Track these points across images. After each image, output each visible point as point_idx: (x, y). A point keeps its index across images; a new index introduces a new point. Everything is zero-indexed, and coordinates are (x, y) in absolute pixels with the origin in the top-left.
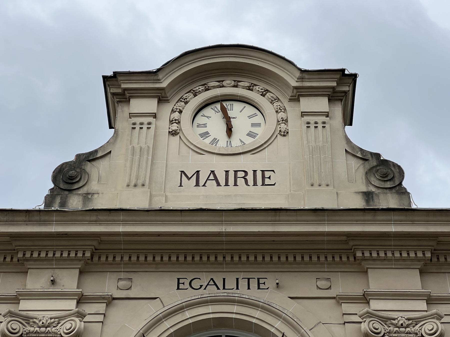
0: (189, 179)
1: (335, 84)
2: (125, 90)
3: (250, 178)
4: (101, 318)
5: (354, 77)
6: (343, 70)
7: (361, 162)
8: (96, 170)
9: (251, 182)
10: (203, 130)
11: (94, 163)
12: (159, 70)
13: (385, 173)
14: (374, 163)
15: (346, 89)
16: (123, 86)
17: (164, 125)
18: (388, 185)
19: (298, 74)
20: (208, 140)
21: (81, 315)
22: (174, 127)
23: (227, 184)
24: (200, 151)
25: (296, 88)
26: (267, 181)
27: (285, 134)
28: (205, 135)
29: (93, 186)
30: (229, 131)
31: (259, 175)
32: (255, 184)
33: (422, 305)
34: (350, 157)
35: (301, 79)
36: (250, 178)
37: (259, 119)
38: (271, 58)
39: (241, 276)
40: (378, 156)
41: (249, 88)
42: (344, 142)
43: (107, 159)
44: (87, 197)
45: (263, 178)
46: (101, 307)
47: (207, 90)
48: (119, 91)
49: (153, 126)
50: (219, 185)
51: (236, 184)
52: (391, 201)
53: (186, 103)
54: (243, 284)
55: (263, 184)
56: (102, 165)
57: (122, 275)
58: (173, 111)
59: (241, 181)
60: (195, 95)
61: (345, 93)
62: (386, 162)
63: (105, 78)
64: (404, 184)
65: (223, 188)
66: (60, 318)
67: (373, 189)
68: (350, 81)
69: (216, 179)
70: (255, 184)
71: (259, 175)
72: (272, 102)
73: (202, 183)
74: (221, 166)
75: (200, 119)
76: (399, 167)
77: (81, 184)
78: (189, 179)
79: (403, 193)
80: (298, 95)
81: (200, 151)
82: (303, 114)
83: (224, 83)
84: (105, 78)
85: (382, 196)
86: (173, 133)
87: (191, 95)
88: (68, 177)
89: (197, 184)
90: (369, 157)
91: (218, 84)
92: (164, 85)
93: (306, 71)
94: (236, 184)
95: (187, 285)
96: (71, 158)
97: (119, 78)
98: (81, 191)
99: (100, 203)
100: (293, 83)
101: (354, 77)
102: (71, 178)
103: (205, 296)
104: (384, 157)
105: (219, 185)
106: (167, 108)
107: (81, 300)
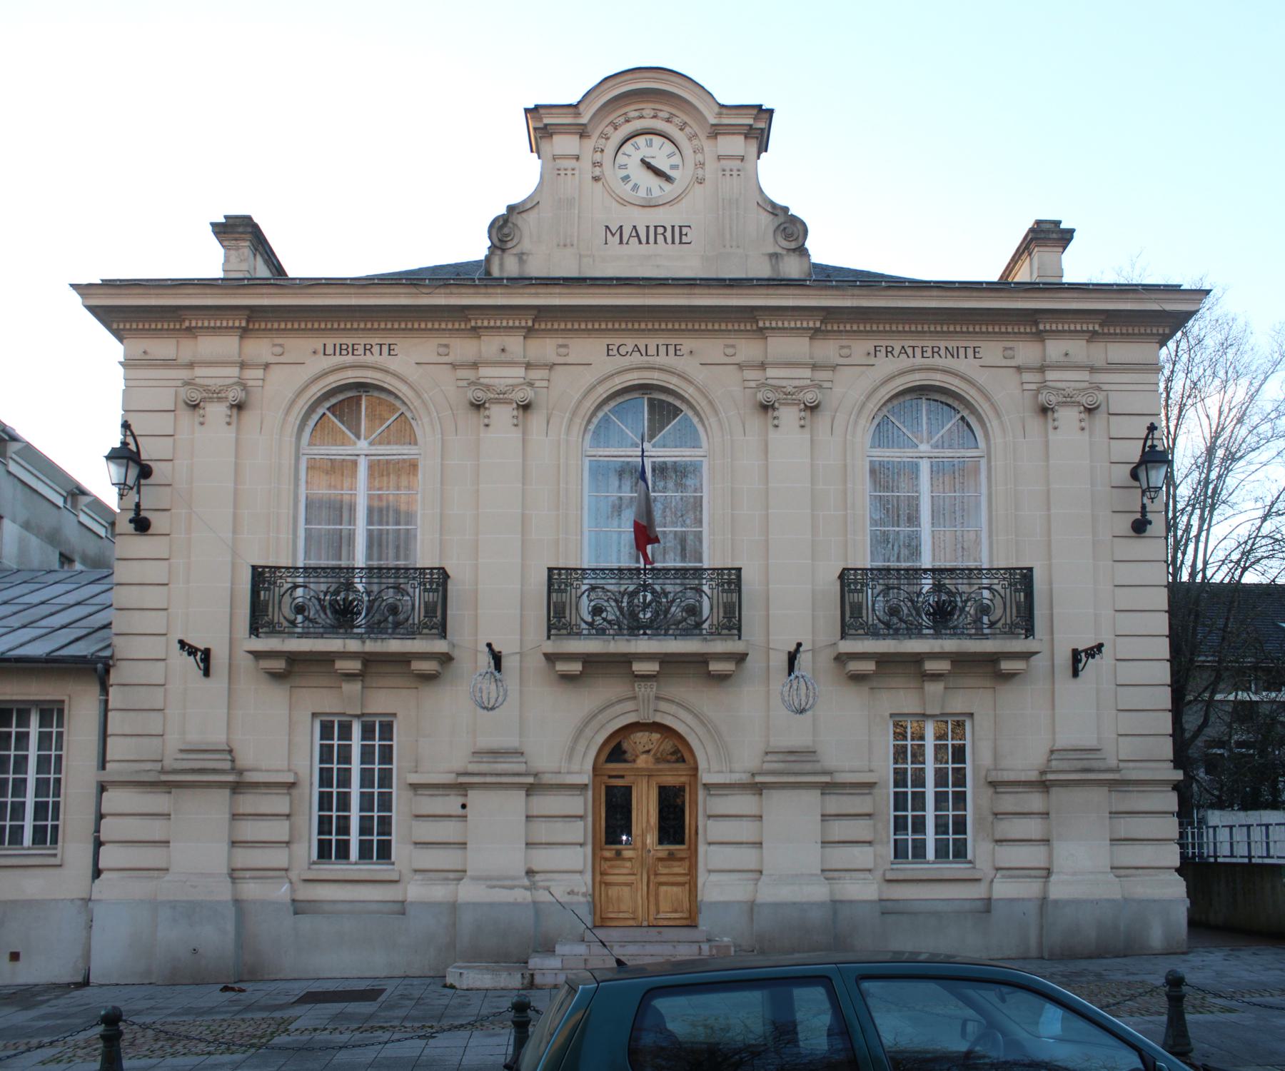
0: (613, 235)
1: (751, 121)
2: (546, 125)
3: (669, 234)
4: (545, 384)
5: (771, 112)
6: (761, 106)
7: (772, 217)
8: (528, 223)
9: (669, 240)
10: (623, 173)
11: (524, 215)
12: (579, 102)
13: (791, 229)
14: (781, 219)
15: (762, 125)
16: (546, 121)
17: (586, 164)
18: (793, 245)
19: (717, 109)
20: (630, 185)
21: (531, 385)
22: (597, 172)
23: (648, 242)
24: (624, 203)
25: (713, 125)
26: (684, 239)
27: (701, 182)
28: (626, 179)
29: (526, 245)
30: (649, 166)
31: (677, 230)
32: (673, 242)
33: (807, 373)
34: (761, 210)
35: (720, 115)
36: (669, 234)
37: (676, 160)
38: (691, 86)
39: (661, 342)
40: (786, 209)
41: (668, 120)
42: (758, 192)
43: (535, 211)
44: (521, 257)
45: (679, 235)
46: (542, 373)
47: (628, 121)
48: (541, 125)
49: (576, 172)
50: (640, 242)
51: (656, 242)
52: (792, 268)
53: (607, 139)
54: (662, 350)
55: (681, 243)
56: (531, 217)
57: (561, 341)
58: (595, 151)
59: (660, 238)
60: (616, 129)
61: (762, 130)
62: (795, 220)
63: (527, 110)
64: (807, 245)
65: (644, 246)
66: (513, 386)
67: (779, 250)
68: (767, 116)
69: (638, 236)
70: (673, 242)
71: (677, 230)
72: (690, 139)
73: (625, 240)
74: (644, 219)
75: (621, 159)
76: (803, 224)
77: (514, 242)
78: (613, 235)
79: (802, 251)
80: (716, 132)
81: (624, 203)
82: (719, 158)
83: (644, 113)
84: (527, 110)
85: (786, 259)
86: (596, 179)
87: (610, 129)
88: (503, 230)
89: (621, 242)
90: (778, 212)
91: (637, 114)
92: (584, 120)
93: (723, 106)
94: (656, 242)
95: (615, 352)
96: (503, 211)
97: (542, 111)
98: (514, 251)
99: (535, 268)
100: (713, 121)
101: (771, 112)
102: (507, 235)
103: (621, 915)
104: (792, 211)
105: (640, 242)
106: (589, 144)
107: (528, 366)
